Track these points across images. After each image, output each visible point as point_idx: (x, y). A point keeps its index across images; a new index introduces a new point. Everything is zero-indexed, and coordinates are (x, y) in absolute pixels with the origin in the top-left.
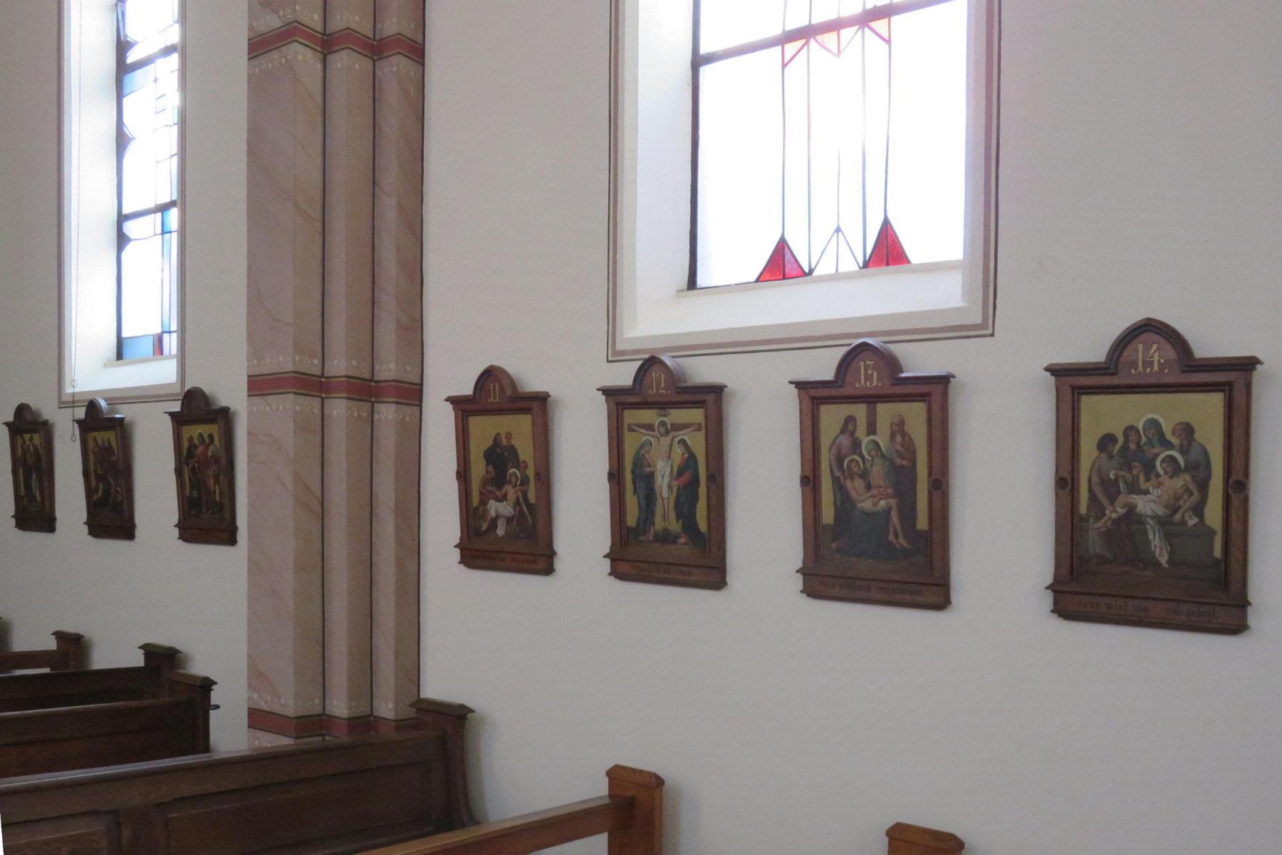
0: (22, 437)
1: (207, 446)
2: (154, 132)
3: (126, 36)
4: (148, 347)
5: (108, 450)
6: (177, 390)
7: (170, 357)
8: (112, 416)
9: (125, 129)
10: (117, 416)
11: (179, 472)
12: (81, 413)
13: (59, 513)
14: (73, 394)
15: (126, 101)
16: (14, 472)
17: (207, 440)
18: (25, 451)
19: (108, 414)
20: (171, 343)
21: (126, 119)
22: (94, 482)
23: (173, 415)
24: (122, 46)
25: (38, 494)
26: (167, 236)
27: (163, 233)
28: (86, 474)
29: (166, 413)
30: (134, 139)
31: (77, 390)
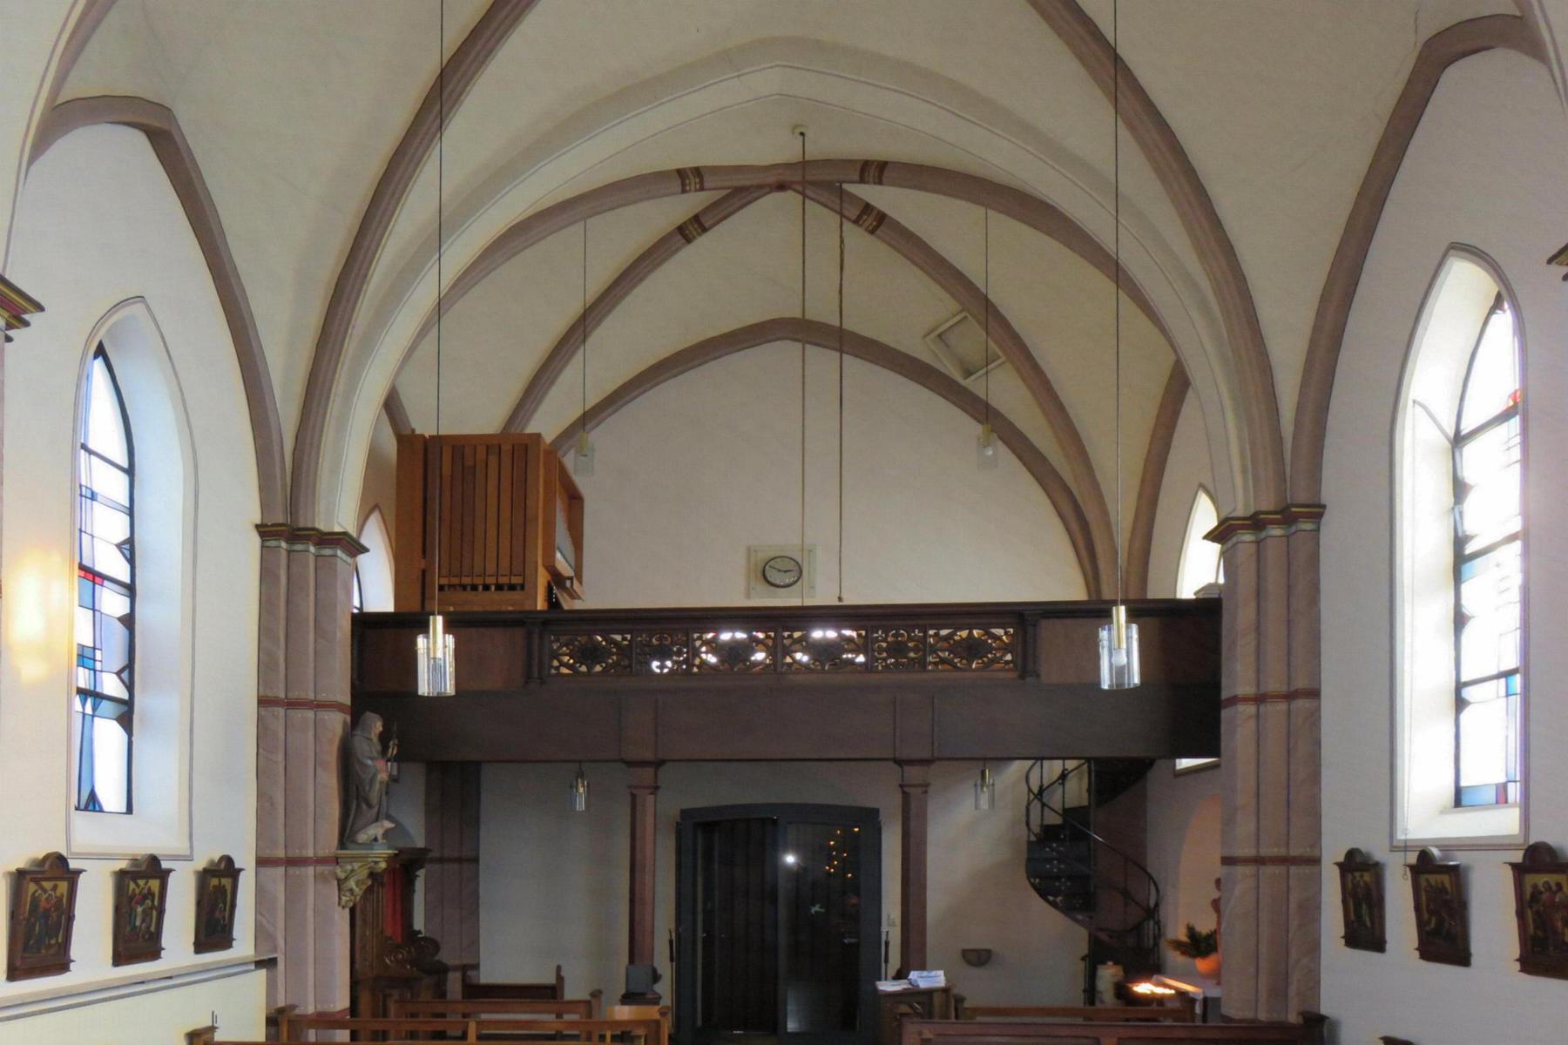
0: (1352, 874)
1: (1555, 893)
2: (1497, 609)
3: (1464, 532)
4: (1491, 796)
5: (1443, 890)
6: (1521, 841)
7: (1513, 806)
8: (1445, 863)
9: (1464, 610)
10: (1451, 863)
11: (1520, 914)
12: (1413, 858)
13: (1388, 936)
14: (1406, 841)
15: (1464, 587)
16: (1344, 901)
17: (1554, 888)
18: (1355, 886)
19: (1441, 860)
20: (1514, 792)
21: (1464, 602)
22: (1426, 916)
23: (1515, 866)
24: (1459, 542)
25: (1367, 919)
26: (1511, 698)
27: (1508, 695)
28: (1417, 909)
29: (1505, 863)
30: (1473, 617)
31: (1410, 836)
